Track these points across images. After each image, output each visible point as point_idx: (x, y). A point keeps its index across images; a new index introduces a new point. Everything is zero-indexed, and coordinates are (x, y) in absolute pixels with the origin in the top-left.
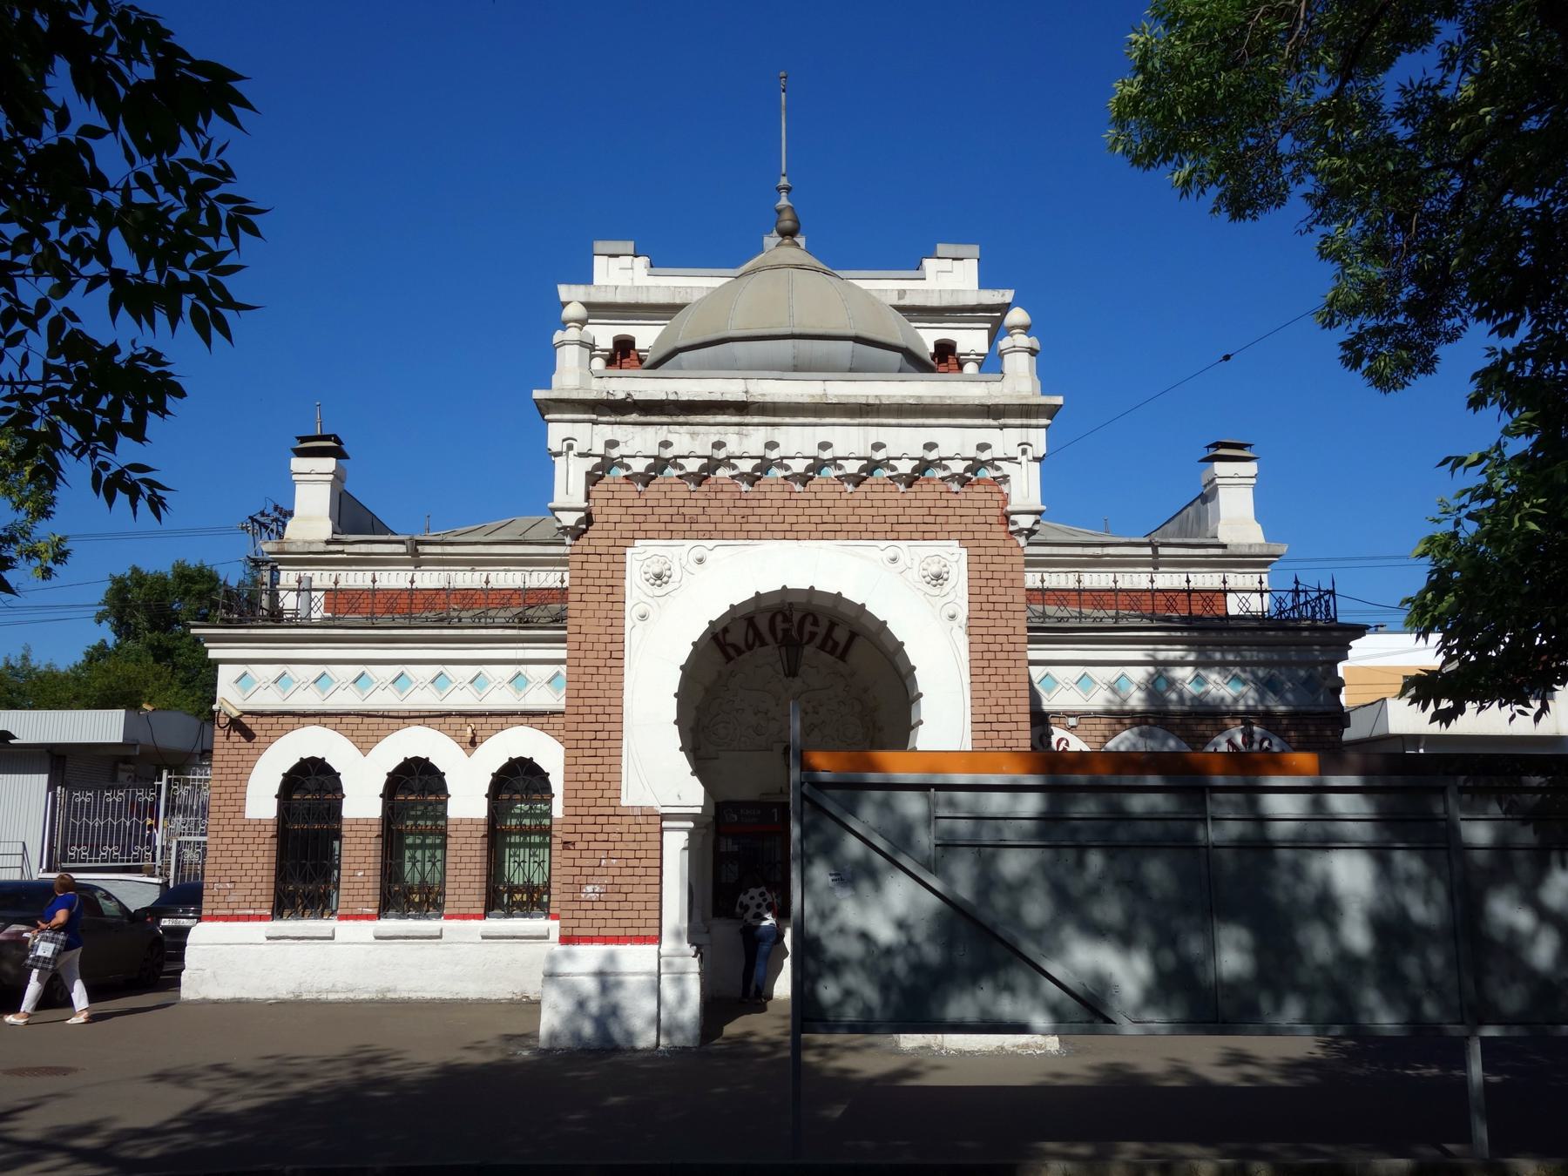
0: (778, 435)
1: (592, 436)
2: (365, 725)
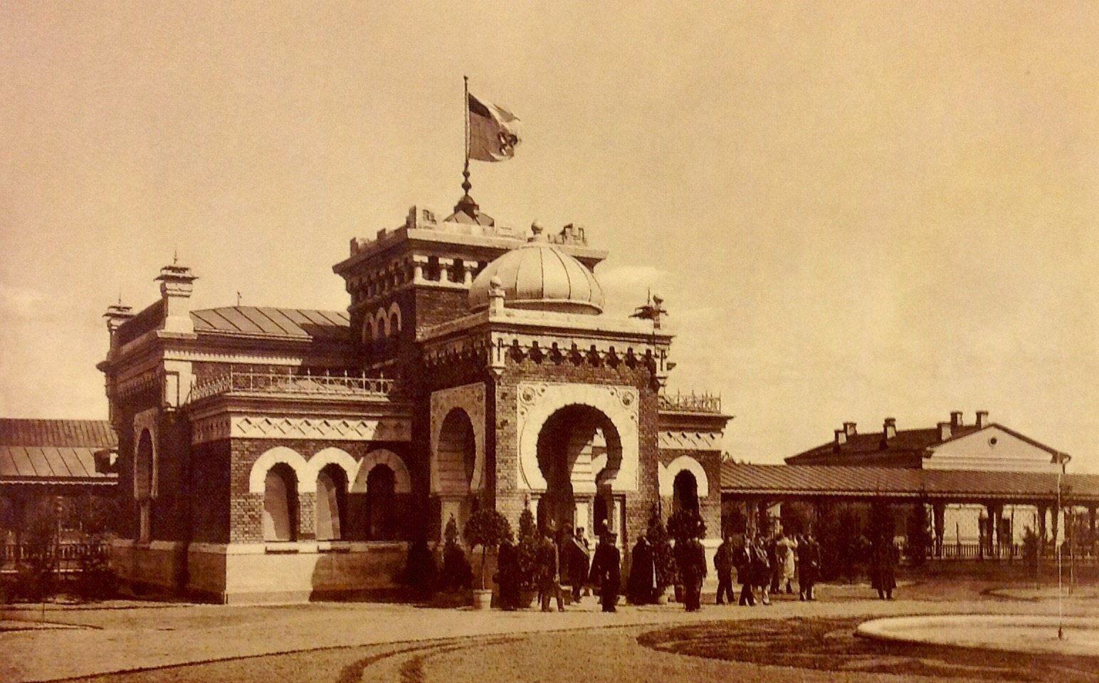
0: (576, 341)
1: (508, 339)
2: (306, 447)
